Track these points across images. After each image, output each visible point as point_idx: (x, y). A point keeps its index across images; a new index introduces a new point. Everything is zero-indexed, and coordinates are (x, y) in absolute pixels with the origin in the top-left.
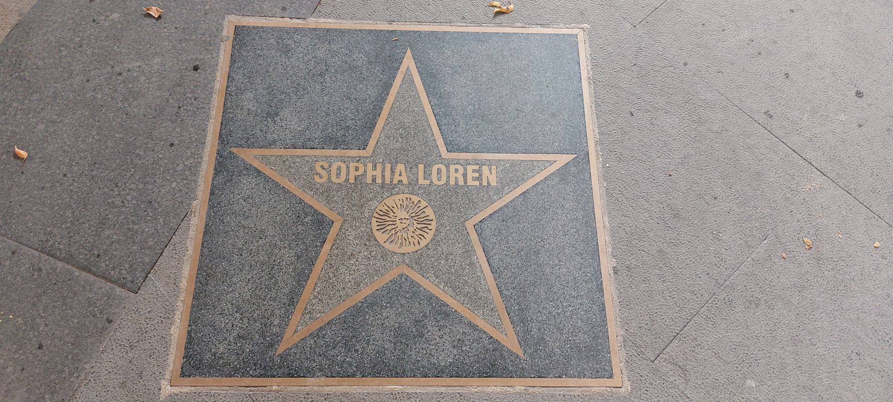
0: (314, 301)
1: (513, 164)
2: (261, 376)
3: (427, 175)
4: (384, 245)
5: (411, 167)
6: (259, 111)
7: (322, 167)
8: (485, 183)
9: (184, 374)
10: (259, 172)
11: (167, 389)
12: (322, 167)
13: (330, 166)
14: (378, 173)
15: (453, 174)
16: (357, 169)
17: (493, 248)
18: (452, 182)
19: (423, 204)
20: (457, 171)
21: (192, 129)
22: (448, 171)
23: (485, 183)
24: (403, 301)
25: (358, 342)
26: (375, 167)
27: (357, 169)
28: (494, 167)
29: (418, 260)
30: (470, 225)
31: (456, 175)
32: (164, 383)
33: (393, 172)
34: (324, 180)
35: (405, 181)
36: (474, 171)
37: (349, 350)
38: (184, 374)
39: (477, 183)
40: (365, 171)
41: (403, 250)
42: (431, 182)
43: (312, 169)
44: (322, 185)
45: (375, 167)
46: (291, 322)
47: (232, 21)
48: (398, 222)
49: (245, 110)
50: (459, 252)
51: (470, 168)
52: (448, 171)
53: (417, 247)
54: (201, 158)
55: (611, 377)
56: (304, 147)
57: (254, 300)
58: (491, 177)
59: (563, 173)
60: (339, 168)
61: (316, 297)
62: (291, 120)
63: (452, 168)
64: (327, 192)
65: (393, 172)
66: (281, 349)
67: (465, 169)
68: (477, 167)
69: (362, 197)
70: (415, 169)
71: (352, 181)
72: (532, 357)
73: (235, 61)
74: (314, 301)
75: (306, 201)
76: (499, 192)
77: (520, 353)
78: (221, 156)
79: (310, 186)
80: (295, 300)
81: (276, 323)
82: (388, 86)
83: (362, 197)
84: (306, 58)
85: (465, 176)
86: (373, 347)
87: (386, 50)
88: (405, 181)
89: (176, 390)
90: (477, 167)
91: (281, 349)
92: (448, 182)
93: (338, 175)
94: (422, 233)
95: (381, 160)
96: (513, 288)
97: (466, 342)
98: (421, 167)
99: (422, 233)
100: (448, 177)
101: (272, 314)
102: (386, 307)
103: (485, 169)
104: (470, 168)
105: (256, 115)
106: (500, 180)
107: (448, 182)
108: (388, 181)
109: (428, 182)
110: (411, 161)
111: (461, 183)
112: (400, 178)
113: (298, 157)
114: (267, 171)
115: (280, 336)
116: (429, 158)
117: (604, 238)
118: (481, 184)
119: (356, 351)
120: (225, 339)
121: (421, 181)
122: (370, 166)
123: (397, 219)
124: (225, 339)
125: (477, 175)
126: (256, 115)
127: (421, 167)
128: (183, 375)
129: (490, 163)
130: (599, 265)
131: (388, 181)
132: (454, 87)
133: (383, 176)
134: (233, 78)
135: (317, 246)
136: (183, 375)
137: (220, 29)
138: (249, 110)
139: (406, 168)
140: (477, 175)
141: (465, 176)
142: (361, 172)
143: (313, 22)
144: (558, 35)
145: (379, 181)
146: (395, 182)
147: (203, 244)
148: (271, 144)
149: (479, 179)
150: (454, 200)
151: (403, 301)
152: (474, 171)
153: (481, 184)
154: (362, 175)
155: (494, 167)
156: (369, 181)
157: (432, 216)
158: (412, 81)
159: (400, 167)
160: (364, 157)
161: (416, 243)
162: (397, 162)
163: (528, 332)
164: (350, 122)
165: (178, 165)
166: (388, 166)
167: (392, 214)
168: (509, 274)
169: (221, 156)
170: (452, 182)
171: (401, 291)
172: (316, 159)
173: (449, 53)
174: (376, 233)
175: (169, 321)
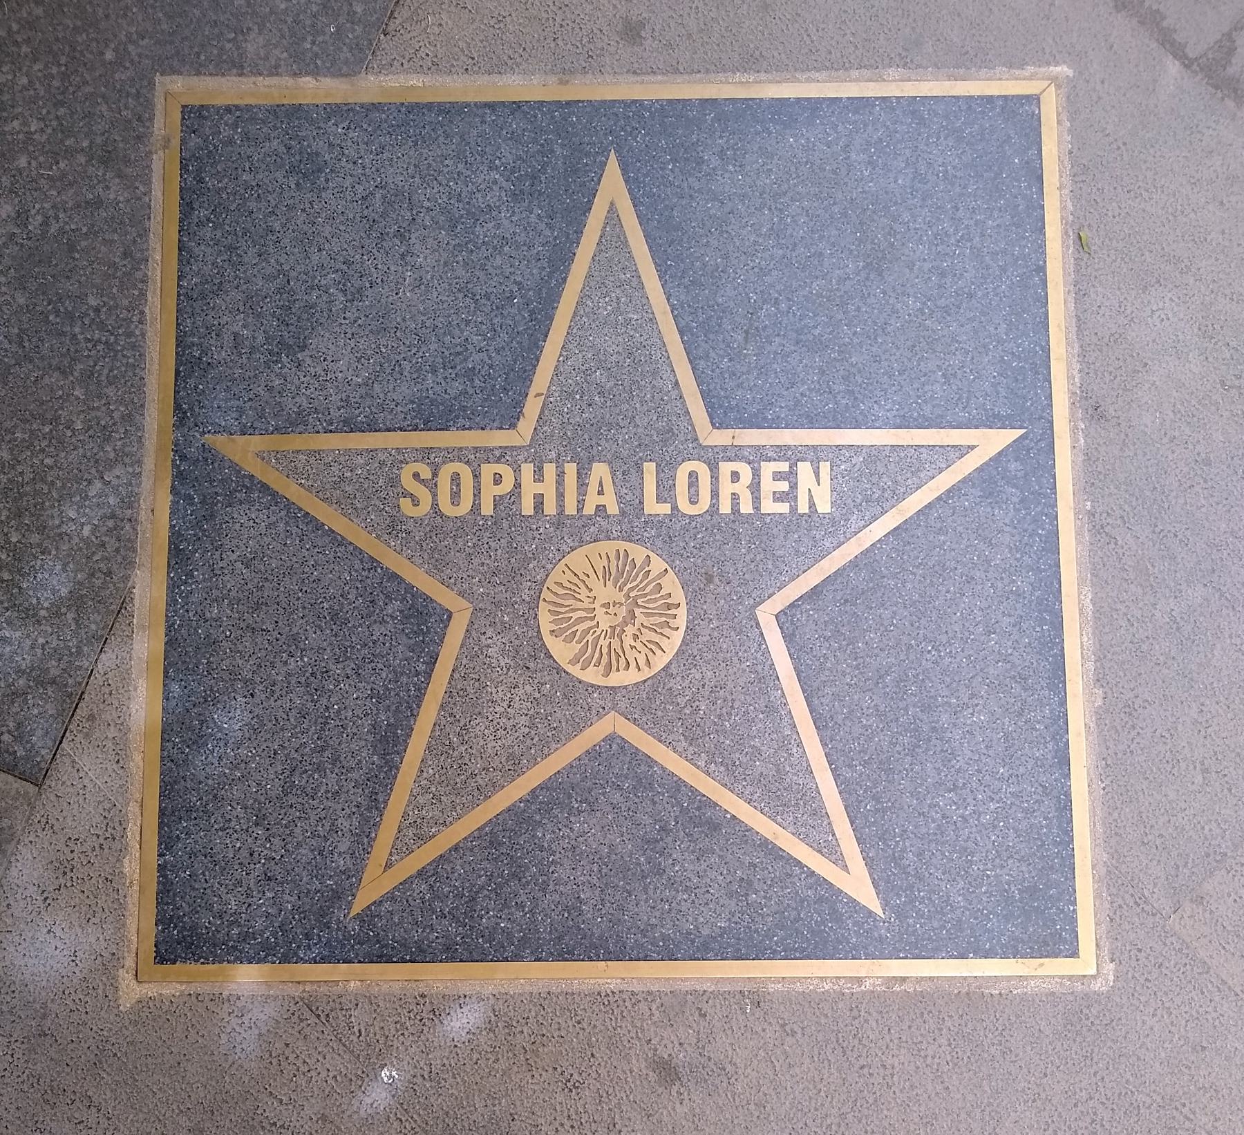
0: (421, 800)
1: (874, 454)
2: (323, 960)
3: (665, 491)
4: (569, 668)
5: (627, 475)
6: (260, 338)
7: (416, 476)
8: (803, 508)
9: (164, 956)
10: (274, 494)
11: (130, 991)
12: (416, 476)
13: (435, 475)
14: (548, 489)
15: (726, 488)
16: (498, 479)
17: (822, 670)
18: (725, 508)
19: (658, 565)
20: (735, 476)
21: (110, 391)
22: (715, 478)
23: (803, 508)
24: (617, 798)
25: (524, 887)
26: (539, 476)
27: (498, 479)
28: (825, 467)
29: (648, 703)
30: (766, 615)
31: (733, 488)
32: (125, 978)
33: (582, 485)
34: (425, 507)
35: (613, 509)
36: (777, 476)
37: (506, 905)
38: (164, 956)
39: (784, 508)
40: (518, 485)
41: (616, 679)
42: (675, 508)
43: (394, 482)
44: (418, 522)
45: (539, 476)
46: (377, 844)
47: (178, 89)
48: (600, 612)
49: (227, 338)
50: (741, 681)
51: (768, 469)
52: (715, 478)
53: (647, 673)
54: (140, 462)
55: (1074, 954)
56: (372, 427)
57: (292, 799)
58: (817, 490)
59: (989, 477)
60: (456, 478)
61: (426, 791)
62: (338, 355)
63: (726, 468)
64: (435, 542)
65: (582, 485)
66: (362, 900)
67: (756, 474)
68: (784, 466)
69: (512, 550)
70: (633, 476)
71: (487, 509)
72: (901, 914)
73: (190, 204)
74: (421, 800)
75: (387, 563)
76: (835, 528)
77: (875, 906)
78: (183, 458)
79: (394, 526)
80: (381, 798)
81: (343, 847)
82: (561, 260)
83: (512, 550)
84: (359, 189)
85: (755, 487)
86: (556, 897)
87: (553, 155)
88: (613, 509)
89: (150, 990)
90: (784, 466)
91: (362, 900)
92: (714, 507)
93: (455, 497)
94: (657, 638)
95: (553, 455)
96: (865, 764)
97: (756, 885)
98: (650, 468)
99: (657, 638)
100: (715, 494)
101: (334, 830)
102: (580, 812)
103: (804, 469)
104: (768, 469)
105: (253, 349)
106: (838, 500)
107: (714, 507)
108: (571, 510)
109: (666, 509)
110: (625, 453)
111: (746, 508)
112: (602, 500)
113: (359, 453)
114: (292, 491)
115: (353, 875)
116: (669, 442)
117: (542, 378)
118: (794, 509)
119: (520, 906)
120: (240, 883)
121: (654, 507)
122: (527, 470)
123: (597, 605)
124: (240, 883)
125: (784, 486)
126: (253, 349)
127: (650, 468)
128: (161, 959)
129: (815, 454)
130: (1063, 702)
131: (571, 510)
132: (726, 257)
133: (560, 496)
134: (190, 252)
135: (417, 674)
136: (161, 959)
137: (144, 117)
138: (236, 335)
139: (613, 474)
140: (784, 486)
141: (755, 487)
142: (507, 486)
143: (373, 86)
144: (990, 99)
145: (550, 509)
146: (589, 510)
147: (166, 672)
148: (297, 422)
149: (789, 496)
150: (726, 559)
151: (617, 798)
152: (777, 476)
153: (794, 509)
154: (511, 494)
155: (825, 467)
156: (527, 508)
157: (679, 596)
158: (623, 243)
159: (600, 471)
160: (513, 448)
161: (642, 662)
162: (591, 460)
163: (896, 860)
164: (477, 357)
165: (90, 482)
166: (571, 469)
167: (584, 591)
168: (857, 730)
169: (183, 458)
170: (725, 508)
171: (616, 765)
172: (401, 457)
173: (715, 161)
174: (549, 641)
175: (117, 845)
